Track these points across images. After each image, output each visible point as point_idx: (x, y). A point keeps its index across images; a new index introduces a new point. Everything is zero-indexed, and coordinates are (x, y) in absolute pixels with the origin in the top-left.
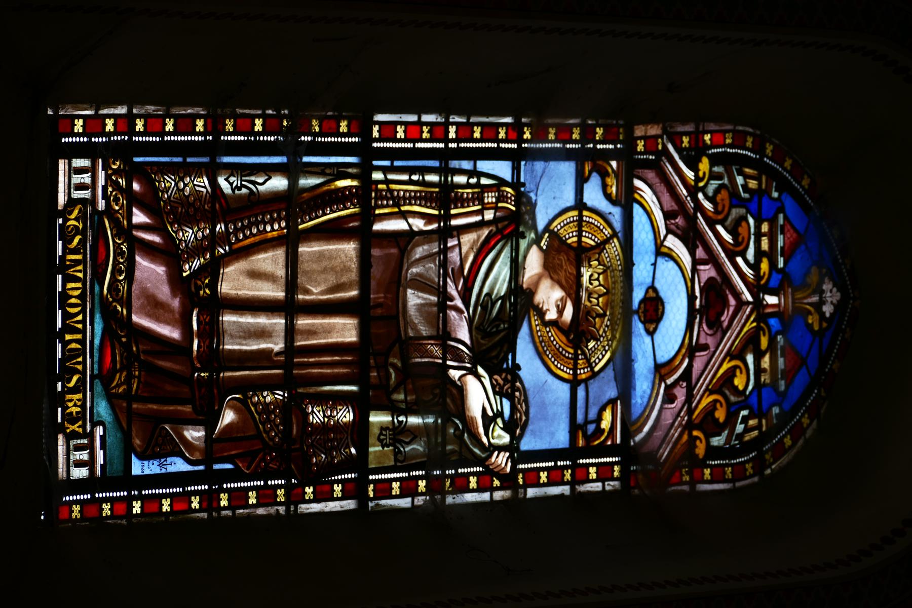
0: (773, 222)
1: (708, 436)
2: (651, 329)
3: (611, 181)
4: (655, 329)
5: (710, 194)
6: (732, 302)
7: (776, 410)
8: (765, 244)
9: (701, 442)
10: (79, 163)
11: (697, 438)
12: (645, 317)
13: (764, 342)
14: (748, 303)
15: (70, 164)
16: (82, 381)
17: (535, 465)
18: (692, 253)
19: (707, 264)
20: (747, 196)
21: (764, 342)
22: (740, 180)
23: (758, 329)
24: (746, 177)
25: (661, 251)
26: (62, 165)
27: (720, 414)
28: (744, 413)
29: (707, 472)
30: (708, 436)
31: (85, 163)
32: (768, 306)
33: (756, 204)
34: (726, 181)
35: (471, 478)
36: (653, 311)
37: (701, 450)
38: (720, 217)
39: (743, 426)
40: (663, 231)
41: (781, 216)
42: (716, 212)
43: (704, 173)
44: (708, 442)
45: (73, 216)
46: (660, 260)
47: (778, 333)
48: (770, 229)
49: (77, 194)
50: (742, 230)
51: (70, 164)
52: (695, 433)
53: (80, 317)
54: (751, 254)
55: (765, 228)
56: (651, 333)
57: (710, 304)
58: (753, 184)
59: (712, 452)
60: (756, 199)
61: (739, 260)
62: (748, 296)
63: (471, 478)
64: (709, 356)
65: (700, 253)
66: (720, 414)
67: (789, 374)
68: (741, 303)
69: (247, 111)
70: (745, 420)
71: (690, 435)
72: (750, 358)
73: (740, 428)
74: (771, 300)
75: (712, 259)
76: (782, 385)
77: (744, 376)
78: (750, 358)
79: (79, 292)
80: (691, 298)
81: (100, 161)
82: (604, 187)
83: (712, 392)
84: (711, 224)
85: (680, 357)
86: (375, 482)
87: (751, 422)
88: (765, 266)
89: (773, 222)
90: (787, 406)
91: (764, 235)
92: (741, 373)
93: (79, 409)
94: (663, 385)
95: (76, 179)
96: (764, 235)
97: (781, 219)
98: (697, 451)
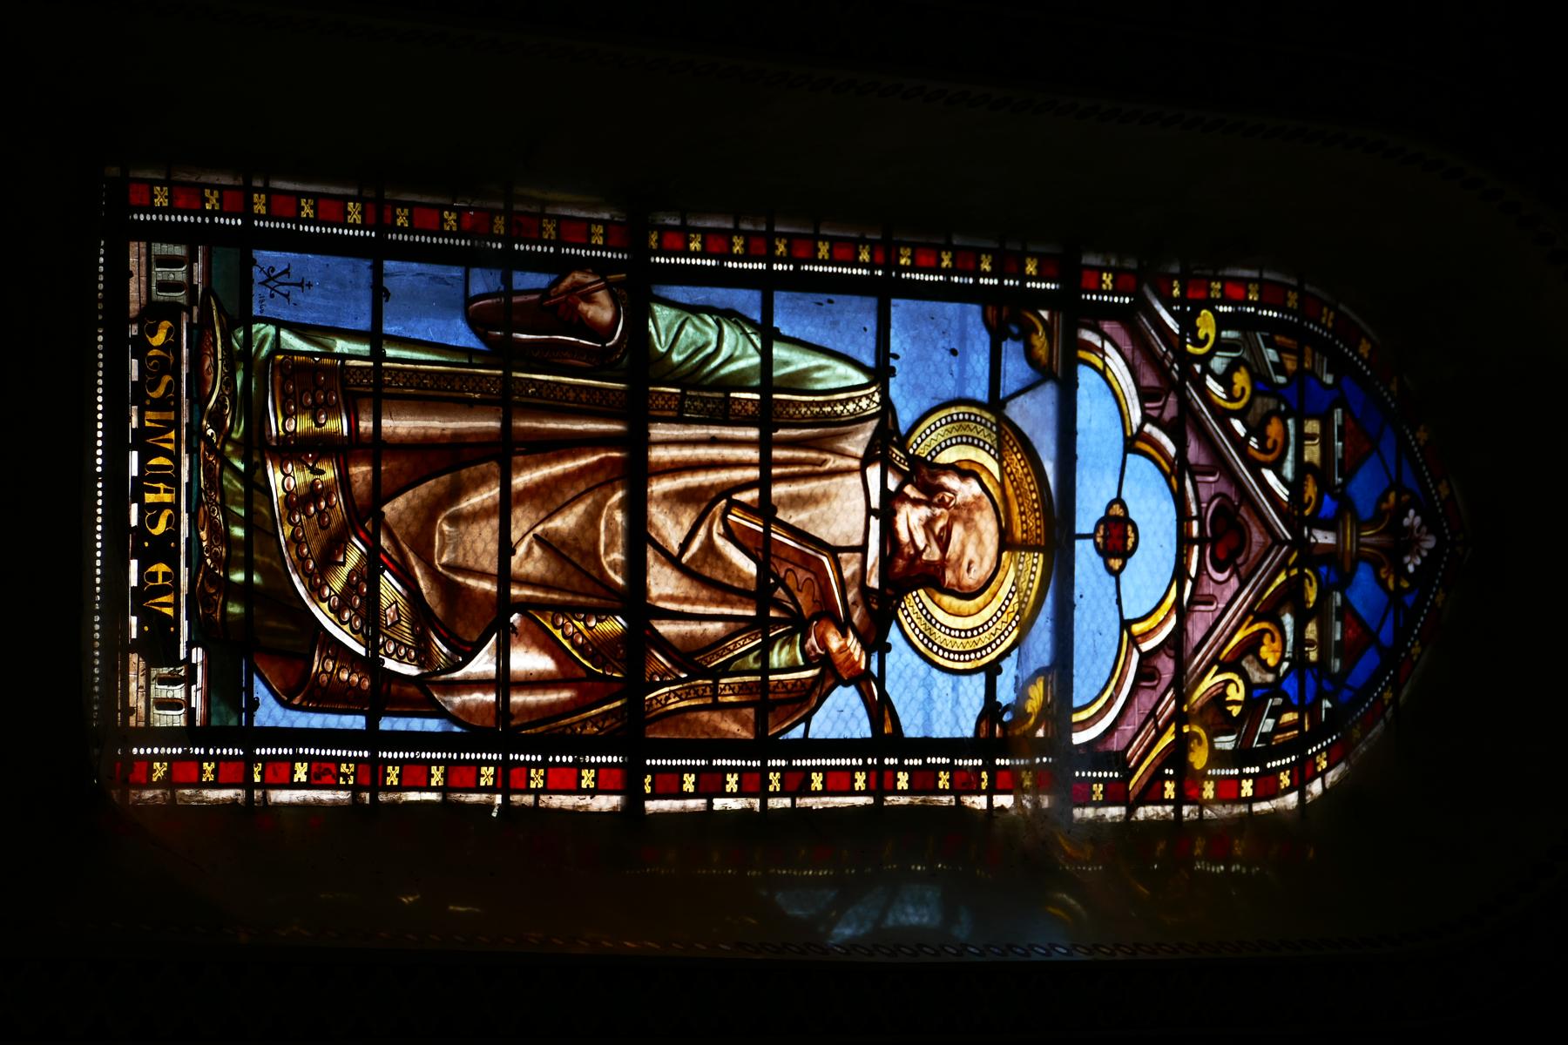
1: (1212, 736)
4: (1122, 567)
6: (1257, 537)
8: (1312, 453)
9: (1200, 742)
10: (160, 249)
13: (1312, 595)
14: (1286, 542)
15: (149, 249)
20: (1281, 379)
21: (1312, 595)
24: (1280, 350)
25: (1133, 443)
28: (1279, 701)
30: (1212, 736)
31: (179, 251)
33: (1298, 399)
35: (814, 775)
36: (1117, 537)
37: (1199, 758)
38: (1270, 458)
39: (1271, 722)
40: (1136, 416)
43: (1275, 442)
44: (1211, 744)
49: (163, 296)
51: (149, 249)
54: (1288, 470)
56: (1116, 574)
57: (1218, 535)
59: (1218, 758)
61: (1269, 475)
63: (814, 775)
64: (1217, 614)
65: (1194, 452)
67: (1348, 650)
68: (1278, 541)
71: (1178, 732)
72: (1288, 620)
73: (1267, 725)
74: (1324, 538)
75: (1220, 464)
76: (1336, 665)
77: (1277, 645)
78: (1288, 620)
80: (1183, 517)
84: (1223, 416)
85: (1160, 615)
86: (654, 770)
87: (1288, 717)
88: (1311, 491)
90: (1346, 695)
91: (1312, 437)
92: (1273, 640)
94: (1135, 657)
95: (160, 273)
96: (1312, 437)
97: (1338, 415)
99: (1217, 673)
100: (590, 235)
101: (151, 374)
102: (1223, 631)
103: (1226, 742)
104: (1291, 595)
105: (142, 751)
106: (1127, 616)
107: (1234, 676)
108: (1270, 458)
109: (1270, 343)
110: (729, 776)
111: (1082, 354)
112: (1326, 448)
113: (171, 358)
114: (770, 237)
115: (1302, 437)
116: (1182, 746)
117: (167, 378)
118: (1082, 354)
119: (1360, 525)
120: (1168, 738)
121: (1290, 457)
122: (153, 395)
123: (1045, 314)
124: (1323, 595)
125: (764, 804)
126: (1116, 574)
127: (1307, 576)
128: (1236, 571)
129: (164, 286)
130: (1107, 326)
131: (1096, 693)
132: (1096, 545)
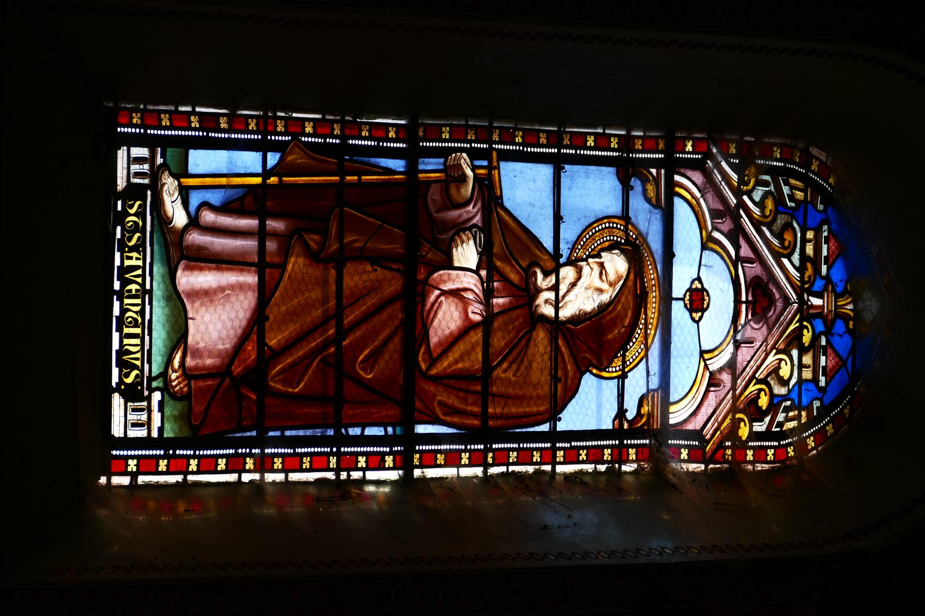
0: (818, 232)
1: (752, 421)
2: (697, 319)
3: (650, 188)
4: (701, 318)
5: (757, 199)
7: (817, 404)
8: (810, 250)
11: (742, 420)
12: (703, 296)
13: (807, 337)
16: (142, 240)
17: (382, 449)
18: (737, 248)
19: (753, 263)
20: (793, 205)
22: (786, 190)
23: (801, 328)
24: (792, 188)
25: (707, 244)
26: (122, 154)
27: (764, 401)
28: (788, 403)
29: (750, 453)
30: (752, 421)
32: (812, 307)
34: (772, 188)
37: (744, 432)
41: (825, 227)
42: (763, 215)
44: (751, 427)
45: (132, 211)
46: (706, 253)
47: (821, 333)
48: (816, 236)
50: (788, 237)
52: (738, 416)
53: (139, 272)
54: (796, 258)
55: (810, 235)
57: (758, 298)
58: (799, 195)
59: (754, 436)
60: (801, 210)
61: (785, 261)
62: (793, 296)
65: (745, 251)
66: (764, 401)
69: (212, 452)
70: (787, 410)
73: (781, 417)
76: (822, 381)
78: (795, 353)
79: (138, 308)
80: (736, 282)
81: (159, 149)
82: (645, 192)
83: (759, 382)
84: (757, 225)
85: (727, 341)
86: (420, 452)
89: (818, 232)
90: (827, 401)
91: (810, 241)
93: (138, 287)
94: (707, 374)
95: (135, 168)
96: (810, 241)
98: (740, 433)
99: (776, 354)
100: (302, 463)
101: (128, 232)
102: (778, 328)
103: (759, 427)
104: (795, 339)
105: (133, 130)
106: (704, 348)
107: (763, 387)
108: (785, 252)
109: (787, 183)
110: (593, 144)
111: (677, 189)
112: (818, 249)
113: (141, 224)
114: (490, 130)
115: (804, 241)
116: (736, 424)
117: (138, 235)
118: (677, 189)
119: (838, 296)
120: (728, 421)
121: (798, 250)
122: (131, 244)
123: (654, 171)
124: (815, 338)
125: (485, 472)
126: (697, 322)
127: (807, 327)
128: (767, 322)
129: (137, 174)
130: (690, 173)
131: (723, 338)
132: (685, 305)
